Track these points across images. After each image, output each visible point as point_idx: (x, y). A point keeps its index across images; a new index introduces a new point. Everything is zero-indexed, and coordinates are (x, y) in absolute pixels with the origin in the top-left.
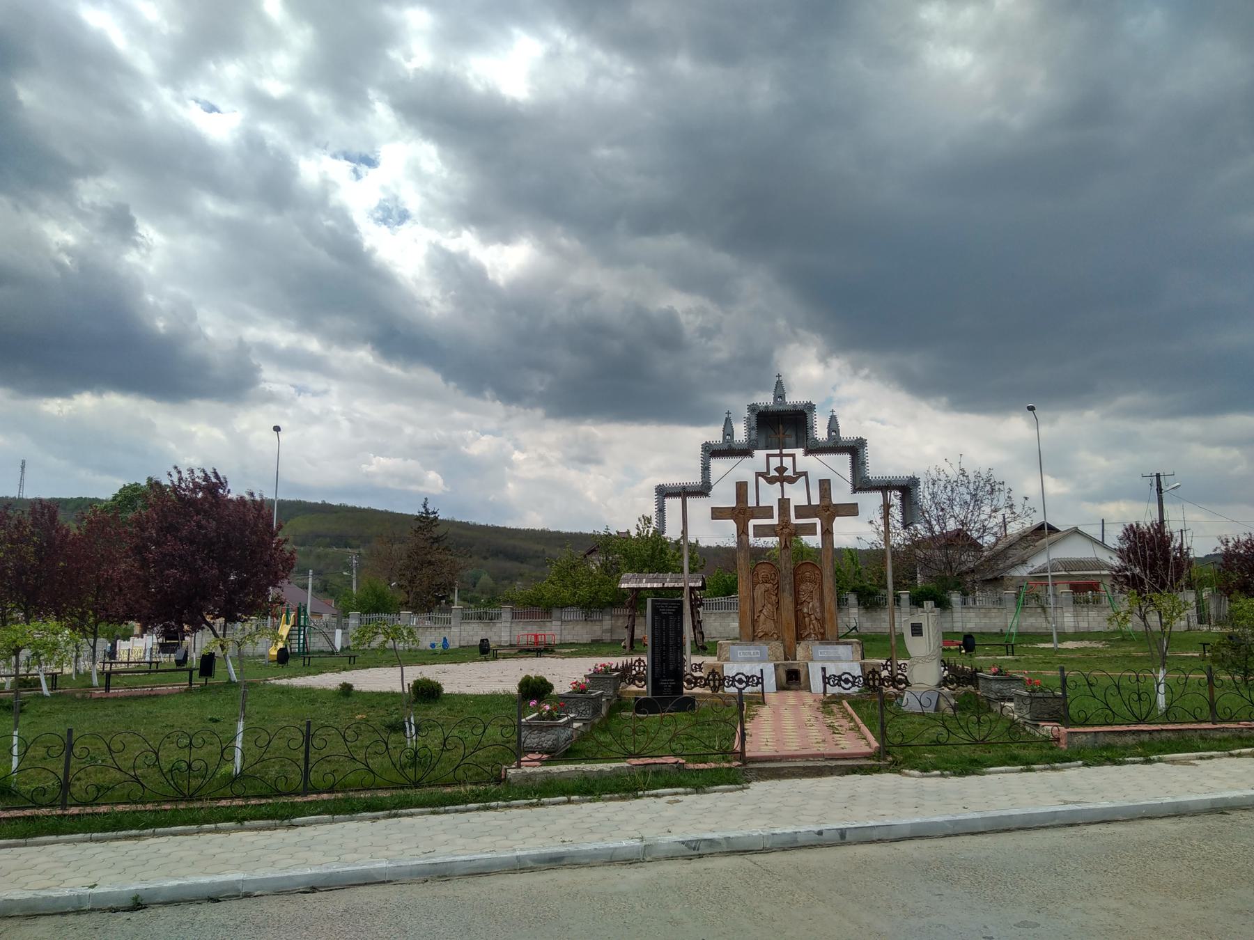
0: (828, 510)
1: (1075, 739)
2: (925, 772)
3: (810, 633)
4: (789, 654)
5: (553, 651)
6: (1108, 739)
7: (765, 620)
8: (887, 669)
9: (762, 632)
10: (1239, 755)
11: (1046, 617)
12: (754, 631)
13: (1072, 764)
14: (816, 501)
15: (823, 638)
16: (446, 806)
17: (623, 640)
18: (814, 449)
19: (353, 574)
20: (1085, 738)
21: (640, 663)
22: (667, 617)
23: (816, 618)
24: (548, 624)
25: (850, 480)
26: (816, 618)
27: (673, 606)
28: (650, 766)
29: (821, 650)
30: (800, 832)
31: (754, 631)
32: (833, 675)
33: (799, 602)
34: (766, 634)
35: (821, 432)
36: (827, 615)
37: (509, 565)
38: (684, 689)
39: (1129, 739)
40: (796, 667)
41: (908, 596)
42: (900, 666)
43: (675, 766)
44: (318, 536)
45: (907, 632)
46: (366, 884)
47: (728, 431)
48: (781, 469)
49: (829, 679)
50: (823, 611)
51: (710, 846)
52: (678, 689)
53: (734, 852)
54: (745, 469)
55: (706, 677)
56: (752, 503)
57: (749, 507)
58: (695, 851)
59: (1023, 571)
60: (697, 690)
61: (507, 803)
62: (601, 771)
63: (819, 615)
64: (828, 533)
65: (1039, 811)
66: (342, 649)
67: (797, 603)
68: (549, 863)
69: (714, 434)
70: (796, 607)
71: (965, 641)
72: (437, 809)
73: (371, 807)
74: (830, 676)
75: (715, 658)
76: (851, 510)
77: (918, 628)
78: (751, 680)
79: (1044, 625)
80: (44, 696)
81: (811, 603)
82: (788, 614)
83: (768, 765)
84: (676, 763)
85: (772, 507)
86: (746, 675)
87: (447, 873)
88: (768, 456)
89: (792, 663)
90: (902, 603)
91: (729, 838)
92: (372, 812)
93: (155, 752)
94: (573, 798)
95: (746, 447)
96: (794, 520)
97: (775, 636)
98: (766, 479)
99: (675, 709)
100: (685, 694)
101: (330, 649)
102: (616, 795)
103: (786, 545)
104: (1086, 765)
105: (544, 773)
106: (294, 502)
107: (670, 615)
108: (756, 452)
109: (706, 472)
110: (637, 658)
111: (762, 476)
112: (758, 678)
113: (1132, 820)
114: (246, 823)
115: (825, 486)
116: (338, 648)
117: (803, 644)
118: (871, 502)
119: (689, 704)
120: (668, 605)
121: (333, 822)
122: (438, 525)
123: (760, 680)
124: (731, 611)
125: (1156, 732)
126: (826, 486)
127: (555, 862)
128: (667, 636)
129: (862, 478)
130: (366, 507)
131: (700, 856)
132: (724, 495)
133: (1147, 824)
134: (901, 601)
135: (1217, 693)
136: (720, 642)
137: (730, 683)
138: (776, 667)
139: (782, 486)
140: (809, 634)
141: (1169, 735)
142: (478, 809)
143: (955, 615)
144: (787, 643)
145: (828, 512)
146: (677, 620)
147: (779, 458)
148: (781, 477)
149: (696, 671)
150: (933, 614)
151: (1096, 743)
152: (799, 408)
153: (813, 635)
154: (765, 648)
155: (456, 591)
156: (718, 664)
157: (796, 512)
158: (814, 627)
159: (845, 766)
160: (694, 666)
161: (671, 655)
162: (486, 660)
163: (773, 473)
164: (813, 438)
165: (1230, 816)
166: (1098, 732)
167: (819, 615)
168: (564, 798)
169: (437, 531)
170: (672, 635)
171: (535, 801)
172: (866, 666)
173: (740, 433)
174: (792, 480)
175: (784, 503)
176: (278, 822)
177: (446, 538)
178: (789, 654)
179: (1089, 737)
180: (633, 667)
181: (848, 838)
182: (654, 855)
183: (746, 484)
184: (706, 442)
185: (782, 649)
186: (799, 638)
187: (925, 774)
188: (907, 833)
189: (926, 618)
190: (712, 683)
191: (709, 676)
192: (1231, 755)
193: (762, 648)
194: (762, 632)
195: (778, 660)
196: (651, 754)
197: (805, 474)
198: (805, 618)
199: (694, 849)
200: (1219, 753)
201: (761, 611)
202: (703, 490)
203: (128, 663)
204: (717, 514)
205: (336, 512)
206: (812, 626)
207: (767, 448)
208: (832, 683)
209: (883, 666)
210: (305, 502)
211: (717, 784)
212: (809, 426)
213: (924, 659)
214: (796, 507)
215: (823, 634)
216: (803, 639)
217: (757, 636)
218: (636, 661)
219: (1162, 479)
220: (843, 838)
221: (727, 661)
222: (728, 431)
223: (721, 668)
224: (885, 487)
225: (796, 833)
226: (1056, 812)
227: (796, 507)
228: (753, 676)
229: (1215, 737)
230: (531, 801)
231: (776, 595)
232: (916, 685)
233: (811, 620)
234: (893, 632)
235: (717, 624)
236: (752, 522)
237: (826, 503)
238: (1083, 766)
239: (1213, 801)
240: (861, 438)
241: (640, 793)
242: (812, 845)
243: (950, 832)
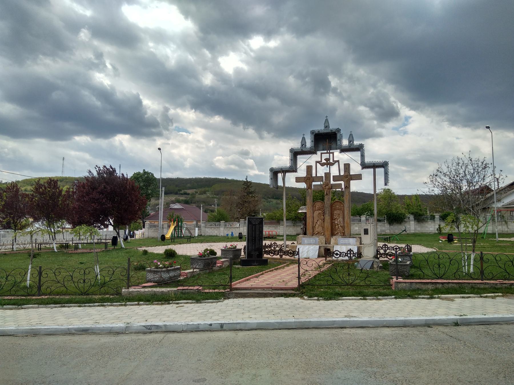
1: (399, 285)
2: (310, 297)
5: (275, 238)
6: (418, 286)
7: (318, 227)
8: (383, 249)
10: (486, 297)
11: (507, 226)
12: (313, 231)
13: (389, 297)
14: (342, 173)
15: (344, 235)
16: (85, 303)
18: (344, 150)
19: (215, 206)
20: (405, 285)
21: (275, 244)
22: (255, 225)
23: (341, 226)
24: (279, 227)
26: (341, 226)
28: (185, 290)
29: (342, 240)
30: (201, 324)
31: (313, 231)
33: (334, 219)
34: (318, 233)
36: (346, 225)
39: (430, 287)
41: (439, 216)
42: (389, 248)
43: (197, 290)
44: (223, 192)
45: (362, 232)
46: (3, 335)
47: (303, 143)
50: (344, 223)
51: (157, 328)
52: (261, 255)
53: (168, 331)
54: (312, 159)
55: (404, 247)
56: (314, 175)
58: (149, 330)
61: (111, 304)
62: (162, 292)
63: (342, 225)
64: (348, 187)
65: (327, 320)
66: (198, 235)
67: (332, 219)
68: (82, 331)
69: (296, 145)
72: (81, 305)
73: (56, 302)
76: (358, 177)
77: (366, 231)
79: (506, 229)
80: (55, 252)
81: (339, 219)
82: (327, 223)
83: (242, 292)
84: (197, 289)
87: (37, 333)
88: (321, 154)
90: (436, 219)
91: (166, 325)
92: (54, 304)
93: (511, 262)
94: (141, 303)
96: (332, 182)
97: (323, 234)
98: (320, 164)
101: (189, 235)
102: (160, 303)
103: (327, 193)
104: (396, 298)
105: (137, 291)
106: (215, 178)
107: (257, 224)
110: (274, 242)
111: (319, 163)
113: (377, 327)
114: (5, 306)
115: (347, 167)
116: (196, 235)
117: (334, 237)
118: (367, 174)
121: (38, 308)
122: (252, 187)
124: (355, 222)
125: (446, 284)
126: (347, 167)
127: (85, 331)
128: (255, 233)
130: (241, 180)
131: (151, 333)
132: (302, 172)
133: (316, 331)
134: (435, 219)
135: (485, 265)
138: (320, 247)
140: (338, 233)
141: (453, 285)
142: (98, 306)
144: (327, 237)
145: (347, 178)
148: (328, 163)
150: (372, 224)
151: (411, 287)
153: (339, 234)
157: (333, 179)
159: (278, 293)
162: (241, 241)
163: (324, 161)
165: (432, 329)
166: (412, 282)
167: (342, 225)
168: (136, 303)
169: (252, 190)
170: (257, 233)
171: (124, 303)
173: (309, 144)
176: (17, 306)
178: (328, 242)
179: (407, 284)
181: (224, 327)
182: (130, 331)
185: (324, 239)
186: (333, 234)
187: (310, 298)
188: (255, 327)
191: (348, 252)
192: (481, 297)
196: (187, 285)
197: (338, 161)
198: (336, 226)
199: (149, 329)
200: (475, 295)
201: (316, 223)
203: (106, 240)
204: (298, 180)
205: (230, 182)
206: (339, 230)
208: (344, 253)
209: (381, 248)
210: (219, 178)
211: (208, 299)
214: (333, 176)
215: (344, 233)
216: (335, 235)
218: (274, 243)
220: (222, 327)
221: (300, 244)
222: (303, 144)
224: (374, 166)
225: (199, 324)
226: (335, 321)
227: (333, 176)
229: (480, 287)
230: (122, 303)
232: (365, 257)
233: (338, 227)
237: (347, 173)
238: (394, 298)
239: (426, 320)
241: (171, 302)
242: (206, 330)
243: (277, 327)
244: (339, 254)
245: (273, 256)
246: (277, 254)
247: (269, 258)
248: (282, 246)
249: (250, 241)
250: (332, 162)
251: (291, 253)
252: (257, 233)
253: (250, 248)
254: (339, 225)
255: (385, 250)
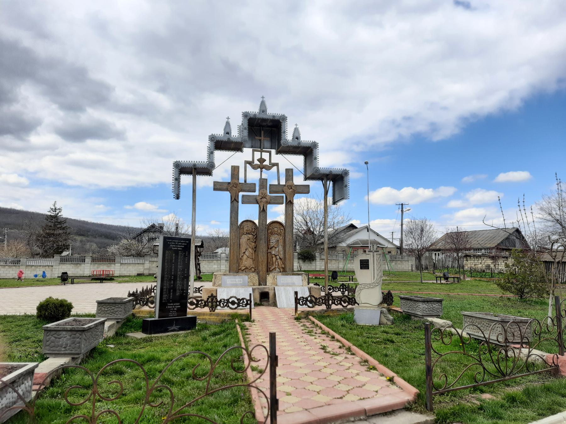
0: (291, 188)
3: (276, 267)
4: (262, 281)
5: (113, 279)
8: (340, 290)
9: (245, 266)
14: (283, 182)
15: (284, 271)
17: (155, 274)
24: (113, 265)
25: (303, 172)
26: (280, 258)
27: (182, 243)
32: (302, 297)
33: (270, 247)
35: (288, 136)
36: (287, 256)
37: (106, 241)
38: (188, 309)
40: (267, 290)
48: (262, 160)
49: (299, 300)
52: (183, 310)
56: (241, 180)
57: (240, 183)
59: (344, 245)
60: (198, 310)
63: (282, 256)
67: (269, 248)
70: (267, 251)
71: (333, 274)
74: (300, 298)
75: (211, 284)
76: (305, 190)
78: (241, 302)
81: (277, 249)
82: (262, 257)
85: (242, 203)
86: (238, 298)
89: (264, 288)
95: (240, 140)
97: (253, 270)
99: (179, 328)
100: (190, 314)
107: (180, 250)
108: (245, 149)
109: (211, 155)
112: (247, 301)
115: (289, 173)
119: (190, 324)
120: (178, 242)
123: (249, 302)
126: (290, 173)
128: (176, 268)
129: (314, 168)
136: (215, 273)
137: (225, 304)
139: (261, 171)
140: (275, 268)
143: (317, 263)
146: (185, 255)
147: (260, 153)
148: (261, 166)
149: (196, 292)
150: (377, 253)
152: (276, 118)
153: (277, 269)
154: (246, 277)
155: (71, 249)
156: (213, 288)
158: (278, 264)
160: (195, 289)
161: (178, 282)
163: (256, 162)
164: (285, 139)
170: (180, 267)
172: (311, 289)
174: (268, 168)
175: (263, 182)
177: (65, 222)
178: (262, 281)
180: (152, 290)
183: (238, 167)
184: (212, 134)
185: (257, 278)
186: (268, 271)
189: (372, 256)
190: (210, 304)
191: (208, 299)
193: (242, 278)
194: (245, 266)
195: (254, 286)
197: (277, 165)
201: (244, 252)
202: (206, 170)
207: (186, 277)
208: (301, 303)
209: (338, 289)
212: (283, 130)
213: (370, 286)
216: (271, 271)
217: (240, 269)
219: (404, 206)
221: (220, 286)
223: (215, 291)
228: (243, 299)
231: (255, 242)
232: (363, 305)
234: (327, 268)
235: (206, 266)
236: (241, 194)
240: (315, 142)
244: (308, 301)
245: (194, 309)
246: (205, 306)
247: (200, 314)
248: (200, 289)
249: (141, 280)
250: (268, 164)
251: (233, 303)
252: (180, 267)
253: (165, 296)
254: (278, 257)
255: (343, 291)
